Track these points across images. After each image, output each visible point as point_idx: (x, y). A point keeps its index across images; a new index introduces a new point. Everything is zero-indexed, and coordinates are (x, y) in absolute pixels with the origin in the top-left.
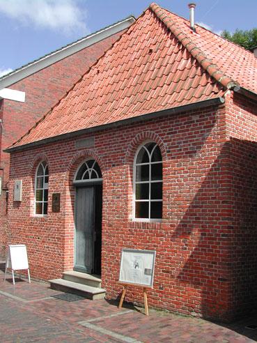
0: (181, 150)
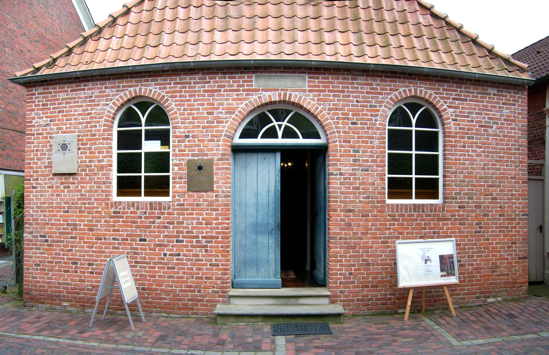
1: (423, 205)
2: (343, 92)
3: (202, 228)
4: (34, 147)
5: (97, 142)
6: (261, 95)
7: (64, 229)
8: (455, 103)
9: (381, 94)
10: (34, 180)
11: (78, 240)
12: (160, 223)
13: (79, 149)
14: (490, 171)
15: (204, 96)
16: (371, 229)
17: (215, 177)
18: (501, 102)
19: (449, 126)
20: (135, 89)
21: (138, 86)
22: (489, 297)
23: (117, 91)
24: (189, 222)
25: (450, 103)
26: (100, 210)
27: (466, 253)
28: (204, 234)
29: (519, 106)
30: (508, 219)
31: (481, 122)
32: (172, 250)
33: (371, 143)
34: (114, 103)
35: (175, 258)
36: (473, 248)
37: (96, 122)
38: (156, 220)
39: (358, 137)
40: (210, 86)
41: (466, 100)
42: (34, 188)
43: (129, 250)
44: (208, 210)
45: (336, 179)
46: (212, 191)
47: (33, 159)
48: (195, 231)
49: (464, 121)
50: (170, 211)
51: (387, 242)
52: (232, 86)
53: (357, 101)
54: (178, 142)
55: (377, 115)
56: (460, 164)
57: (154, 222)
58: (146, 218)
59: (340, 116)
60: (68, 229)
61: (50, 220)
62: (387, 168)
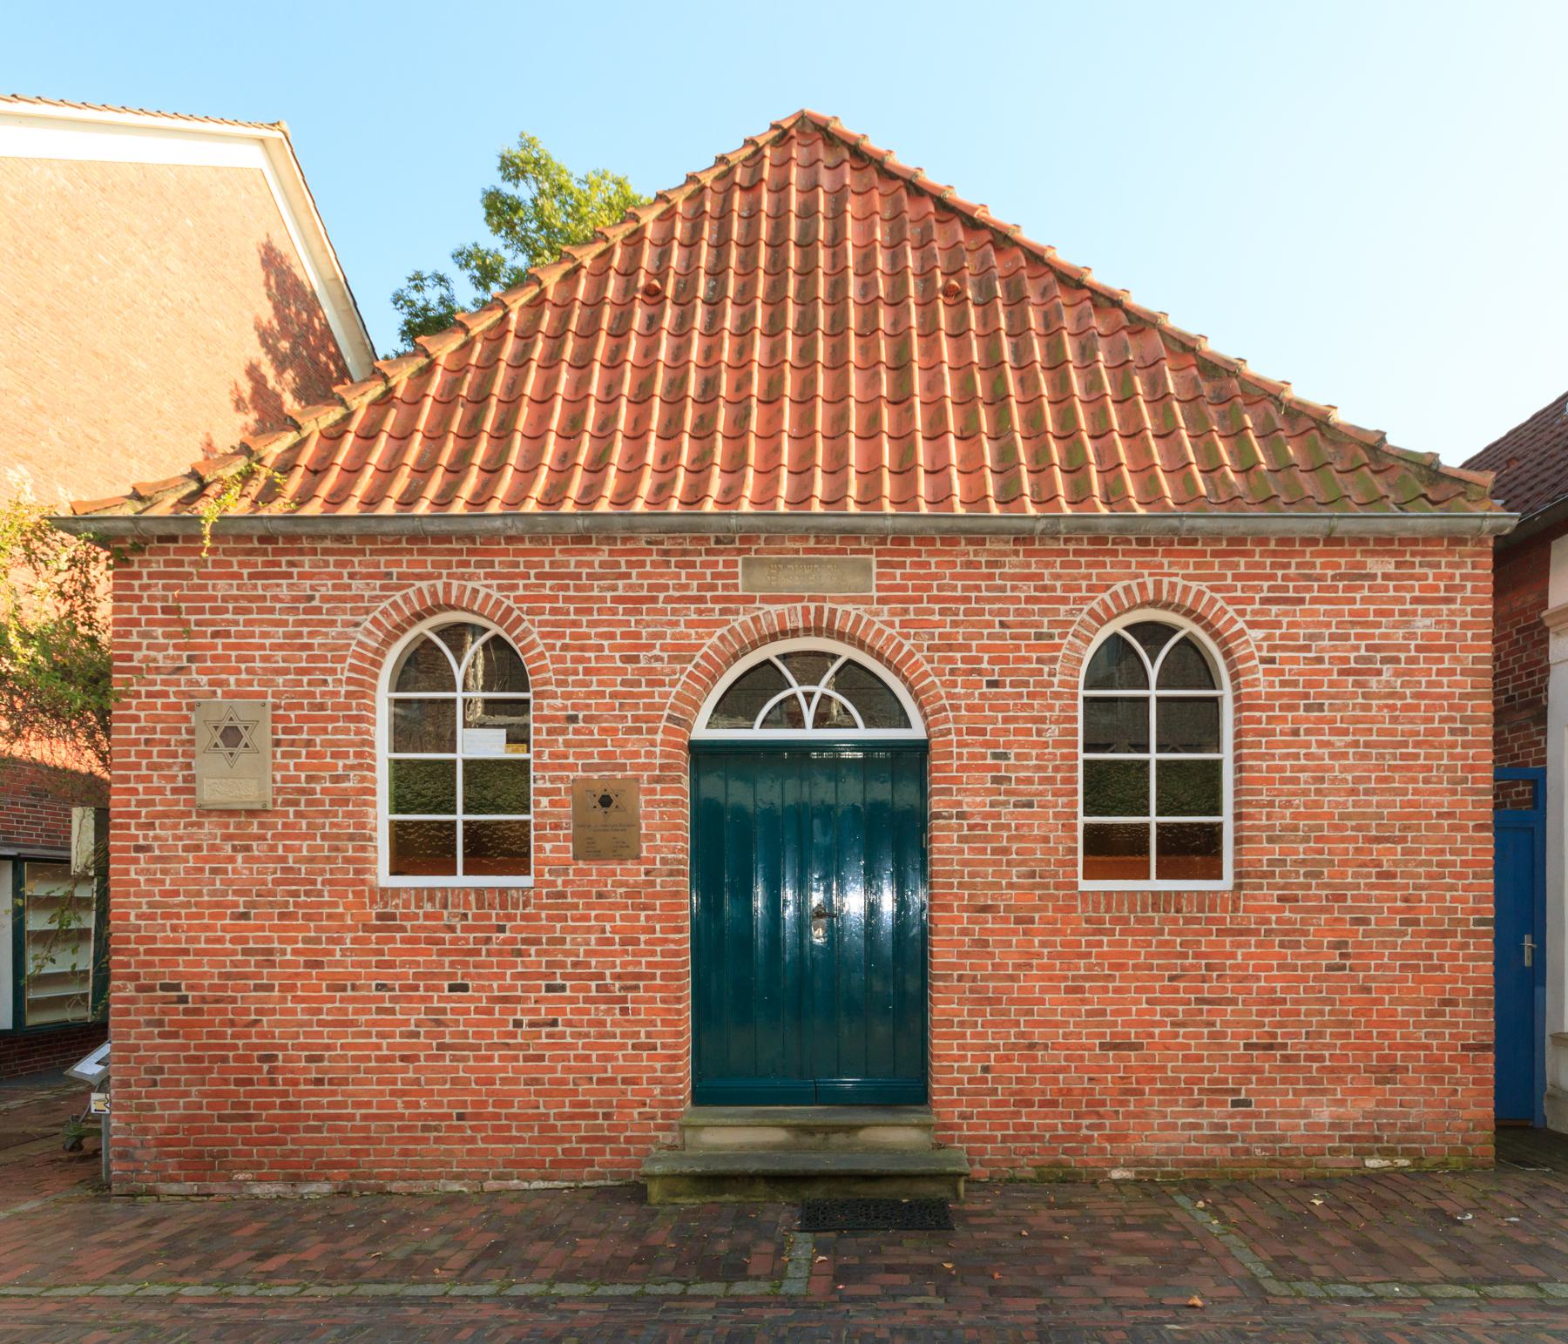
0: (1320, 660)
1: (1179, 893)
2: (967, 600)
3: (613, 954)
4: (140, 731)
5: (330, 726)
6: (760, 613)
7: (234, 964)
8: (1268, 613)
9: (1065, 601)
10: (140, 826)
11: (276, 993)
12: (505, 942)
13: (277, 743)
14: (1375, 799)
15: (614, 612)
16: (1039, 955)
17: (643, 823)
18: (1408, 596)
19: (1250, 677)
20: (434, 586)
21: (439, 576)
22: (1370, 1153)
23: (383, 588)
24: (579, 937)
25: (1254, 613)
26: (341, 910)
27: (1301, 1024)
28: (618, 970)
29: (1465, 601)
30: (1432, 934)
31: (1346, 660)
32: (536, 1011)
33: (1039, 733)
34: (375, 621)
35: (544, 1030)
36: (1321, 1013)
37: (324, 671)
38: (494, 935)
39: (1006, 720)
40: (631, 587)
41: (1301, 601)
42: (139, 849)
43: (422, 1016)
44: (626, 907)
45: (948, 828)
46: (637, 858)
47: (137, 766)
48: (593, 961)
49: (1295, 661)
50: (530, 910)
51: (1081, 990)
52: (685, 587)
53: (1002, 624)
54: (550, 732)
55: (1054, 660)
56: (1283, 781)
57: (488, 940)
58: (466, 929)
59: (960, 665)
60: (246, 964)
61: (190, 940)
62: (1080, 797)
